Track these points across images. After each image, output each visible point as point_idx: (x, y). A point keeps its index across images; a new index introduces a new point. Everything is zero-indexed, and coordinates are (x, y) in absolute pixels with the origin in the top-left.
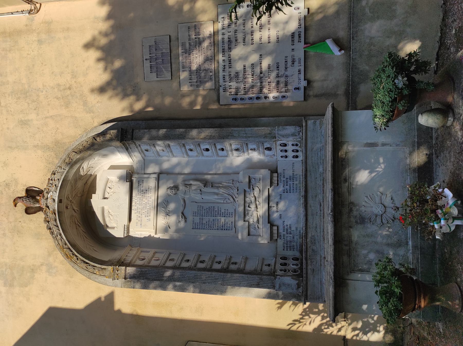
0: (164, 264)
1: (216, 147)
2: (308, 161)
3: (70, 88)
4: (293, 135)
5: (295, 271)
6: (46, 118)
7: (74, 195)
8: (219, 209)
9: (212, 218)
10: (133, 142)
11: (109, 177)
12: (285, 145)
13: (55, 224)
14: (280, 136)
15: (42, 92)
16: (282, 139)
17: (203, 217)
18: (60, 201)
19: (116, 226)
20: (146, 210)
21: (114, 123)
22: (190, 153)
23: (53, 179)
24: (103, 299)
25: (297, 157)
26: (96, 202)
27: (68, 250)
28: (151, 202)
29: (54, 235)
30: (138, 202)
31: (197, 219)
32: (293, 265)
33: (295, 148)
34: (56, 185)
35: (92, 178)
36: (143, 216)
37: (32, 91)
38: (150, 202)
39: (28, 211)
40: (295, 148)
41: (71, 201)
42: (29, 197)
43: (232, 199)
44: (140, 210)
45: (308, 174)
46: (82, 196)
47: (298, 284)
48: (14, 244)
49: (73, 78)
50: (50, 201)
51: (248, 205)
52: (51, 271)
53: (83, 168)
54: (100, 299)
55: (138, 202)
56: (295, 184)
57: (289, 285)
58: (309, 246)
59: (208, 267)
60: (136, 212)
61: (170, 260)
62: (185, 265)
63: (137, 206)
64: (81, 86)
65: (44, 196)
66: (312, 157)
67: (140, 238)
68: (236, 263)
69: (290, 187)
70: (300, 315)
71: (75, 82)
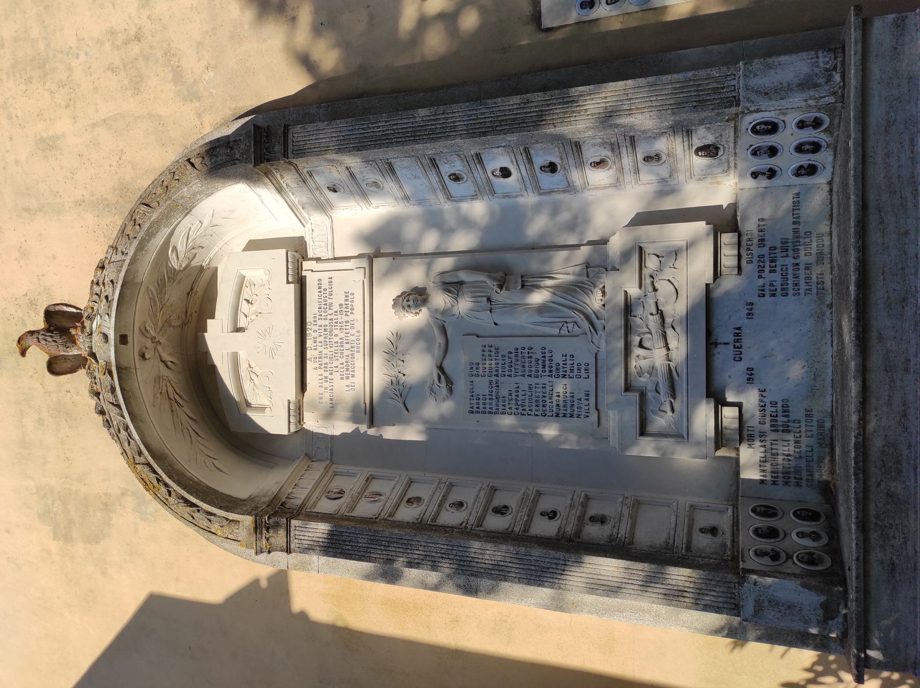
0: (392, 515)
1: (530, 160)
2: (871, 171)
3: (138, 38)
4: (806, 84)
5: (811, 559)
6: (94, 125)
7: (160, 324)
8: (548, 355)
9: (525, 382)
10: (290, 163)
11: (244, 273)
12: (772, 128)
13: (112, 399)
14: (753, 97)
15: (77, 56)
16: (764, 104)
17: (501, 379)
18: (123, 339)
19: (267, 403)
20: (343, 360)
21: (250, 117)
22: (452, 186)
23: (101, 282)
24: (264, 583)
25: (811, 170)
26: (218, 340)
27: (146, 469)
28: (354, 338)
29: (112, 429)
30: (321, 339)
31: (482, 386)
32: (801, 535)
33: (809, 135)
34: (107, 297)
35: (206, 276)
36: (336, 376)
37: (55, 56)
38: (351, 338)
39: (54, 367)
40: (809, 135)
41: (153, 339)
42: (52, 332)
43: (586, 325)
44: (327, 360)
45: (873, 220)
46: (184, 324)
47: (824, 606)
48: (62, 443)
49: (143, 7)
50: (96, 338)
51: (637, 339)
52: (143, 508)
53: (175, 248)
54: (256, 582)
55: (319, 339)
56: (802, 267)
57: (790, 607)
58: (872, 482)
59: (517, 529)
60: (317, 365)
61: (409, 501)
62: (450, 517)
63: (320, 349)
64: (165, 28)
65: (83, 327)
66: (888, 155)
67: (332, 437)
68: (602, 520)
69: (784, 277)
70: (809, 670)
71: (149, 18)
